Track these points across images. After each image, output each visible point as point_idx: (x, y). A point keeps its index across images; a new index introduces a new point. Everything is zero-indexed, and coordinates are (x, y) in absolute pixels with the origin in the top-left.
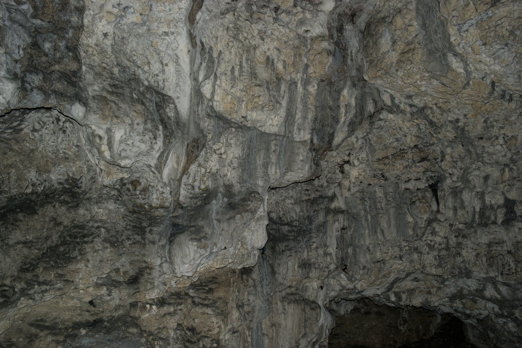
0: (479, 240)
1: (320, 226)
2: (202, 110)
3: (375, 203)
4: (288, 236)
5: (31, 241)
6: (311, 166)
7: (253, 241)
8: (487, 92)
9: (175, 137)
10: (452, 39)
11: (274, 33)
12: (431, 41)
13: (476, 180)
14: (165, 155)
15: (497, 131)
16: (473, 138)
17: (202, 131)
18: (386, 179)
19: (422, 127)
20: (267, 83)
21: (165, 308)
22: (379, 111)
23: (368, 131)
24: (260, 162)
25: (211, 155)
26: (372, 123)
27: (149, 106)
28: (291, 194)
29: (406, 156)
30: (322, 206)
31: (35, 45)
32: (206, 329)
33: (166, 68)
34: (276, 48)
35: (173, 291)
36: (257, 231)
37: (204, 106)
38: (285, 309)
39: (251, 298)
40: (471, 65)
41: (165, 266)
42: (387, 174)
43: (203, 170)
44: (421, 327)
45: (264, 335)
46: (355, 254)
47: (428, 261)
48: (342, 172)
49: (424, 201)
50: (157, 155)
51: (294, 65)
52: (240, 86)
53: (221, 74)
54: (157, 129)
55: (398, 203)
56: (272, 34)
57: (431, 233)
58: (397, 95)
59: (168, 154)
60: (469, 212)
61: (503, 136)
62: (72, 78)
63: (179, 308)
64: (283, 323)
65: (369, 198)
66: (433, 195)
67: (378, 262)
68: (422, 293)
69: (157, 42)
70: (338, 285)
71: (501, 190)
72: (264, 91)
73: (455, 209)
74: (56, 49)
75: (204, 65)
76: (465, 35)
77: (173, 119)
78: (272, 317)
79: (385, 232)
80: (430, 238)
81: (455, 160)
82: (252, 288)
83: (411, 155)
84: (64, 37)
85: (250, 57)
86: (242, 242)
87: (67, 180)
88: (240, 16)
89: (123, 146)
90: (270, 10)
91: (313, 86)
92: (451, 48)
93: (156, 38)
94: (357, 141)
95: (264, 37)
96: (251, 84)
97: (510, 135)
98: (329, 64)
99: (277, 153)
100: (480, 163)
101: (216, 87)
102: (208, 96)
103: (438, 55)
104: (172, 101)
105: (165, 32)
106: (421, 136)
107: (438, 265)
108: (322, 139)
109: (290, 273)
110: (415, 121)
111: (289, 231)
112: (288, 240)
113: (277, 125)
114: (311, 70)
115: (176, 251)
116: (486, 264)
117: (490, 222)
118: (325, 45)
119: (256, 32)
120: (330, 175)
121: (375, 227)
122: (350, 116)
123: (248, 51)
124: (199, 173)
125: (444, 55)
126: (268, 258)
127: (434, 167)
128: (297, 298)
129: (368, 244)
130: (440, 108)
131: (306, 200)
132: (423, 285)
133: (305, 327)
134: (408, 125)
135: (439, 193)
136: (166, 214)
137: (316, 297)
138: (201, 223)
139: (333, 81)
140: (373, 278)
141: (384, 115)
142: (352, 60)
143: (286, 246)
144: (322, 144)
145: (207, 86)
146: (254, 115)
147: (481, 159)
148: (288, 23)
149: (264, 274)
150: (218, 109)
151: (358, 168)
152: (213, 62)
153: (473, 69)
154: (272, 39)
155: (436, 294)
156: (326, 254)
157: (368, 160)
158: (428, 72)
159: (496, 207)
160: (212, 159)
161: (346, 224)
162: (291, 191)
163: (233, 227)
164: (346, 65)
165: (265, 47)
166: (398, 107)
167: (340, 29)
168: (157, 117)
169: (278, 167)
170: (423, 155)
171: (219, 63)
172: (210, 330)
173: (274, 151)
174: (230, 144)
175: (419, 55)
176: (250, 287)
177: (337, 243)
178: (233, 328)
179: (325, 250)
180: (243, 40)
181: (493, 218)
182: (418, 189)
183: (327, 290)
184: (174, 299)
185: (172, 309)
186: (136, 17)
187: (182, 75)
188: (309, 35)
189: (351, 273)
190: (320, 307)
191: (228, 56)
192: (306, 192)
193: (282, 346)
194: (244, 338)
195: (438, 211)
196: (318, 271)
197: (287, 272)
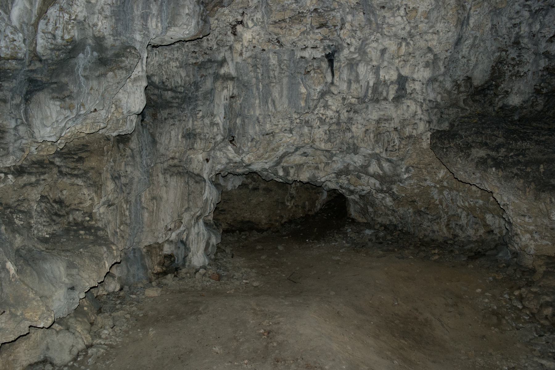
3: (268, 71)
6: (198, 22)
13: (373, 53)
16: (375, 6)
18: (281, 46)
21: (25, 178)
28: (176, 56)
30: (211, 71)
32: (76, 202)
35: (34, 159)
36: (134, 93)
39: (129, 169)
41: (22, 129)
42: (282, 40)
44: (307, 203)
45: (143, 208)
46: (243, 124)
47: (318, 136)
48: (234, 34)
49: (319, 71)
55: (293, 72)
57: (324, 107)
60: (363, 86)
63: (42, 177)
64: (165, 196)
65: (262, 65)
66: (329, 66)
68: (310, 168)
70: (224, 157)
71: (396, 65)
73: (349, 82)
79: (276, 102)
80: (322, 112)
81: (354, 29)
82: (130, 158)
83: (310, 20)
86: (116, 105)
97: (411, 6)
100: (379, 35)
112: (172, 107)
115: (34, 111)
116: (373, 140)
117: (382, 98)
121: (266, 97)
124: (62, 20)
126: (148, 127)
127: (333, 34)
128: (180, 170)
131: (192, 64)
133: (189, 201)
135: (335, 64)
137: (201, 170)
140: (262, 150)
143: (169, 114)
147: (380, 30)
149: (144, 143)
151: (251, 31)
155: (324, 170)
156: (213, 124)
159: (389, 83)
161: (236, 92)
169: (159, 20)
170: (322, 20)
172: (81, 203)
176: (127, 157)
177: (225, 113)
178: (108, 201)
181: (385, 94)
182: (314, 58)
183: (213, 162)
184: (36, 168)
185: (33, 179)
189: (238, 145)
190: (205, 181)
192: (194, 55)
193: (163, 220)
195: (332, 83)
197: (169, 142)
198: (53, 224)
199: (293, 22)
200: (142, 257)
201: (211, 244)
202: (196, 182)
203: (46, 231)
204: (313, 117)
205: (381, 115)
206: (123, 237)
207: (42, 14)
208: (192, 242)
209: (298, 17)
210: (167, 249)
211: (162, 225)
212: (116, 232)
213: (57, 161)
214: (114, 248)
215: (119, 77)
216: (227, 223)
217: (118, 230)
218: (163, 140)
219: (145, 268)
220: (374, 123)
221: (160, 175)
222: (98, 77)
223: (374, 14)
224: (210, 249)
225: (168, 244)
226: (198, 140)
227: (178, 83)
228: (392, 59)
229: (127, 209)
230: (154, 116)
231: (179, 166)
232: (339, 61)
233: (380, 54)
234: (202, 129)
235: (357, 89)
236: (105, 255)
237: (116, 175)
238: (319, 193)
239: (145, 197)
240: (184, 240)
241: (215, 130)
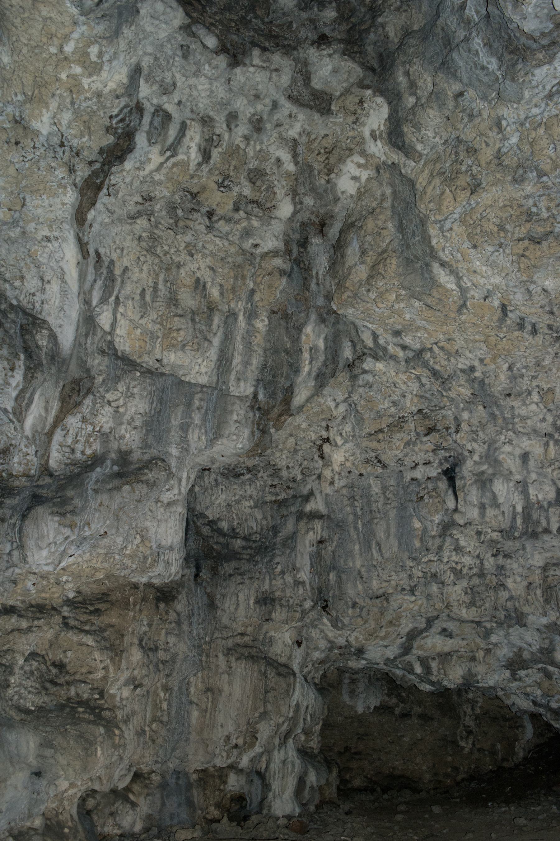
0: (530, 561)
1: (287, 538)
2: (92, 343)
3: (369, 503)
4: (240, 554)
6: (253, 433)
7: (159, 536)
8: (495, 318)
9: (43, 371)
10: (434, 242)
11: (207, 246)
12: (408, 247)
13: (509, 461)
14: (28, 395)
15: (529, 383)
16: (496, 394)
17: (88, 370)
18: (384, 466)
19: (424, 380)
20: (193, 312)
21: (13, 620)
22: (360, 357)
23: (350, 389)
25: (102, 407)
26: (354, 378)
27: (10, 328)
28: (249, 492)
29: (406, 427)
30: (293, 509)
32: (84, 670)
33: (47, 286)
34: (209, 267)
35: (33, 602)
36: (166, 521)
37: (96, 339)
38: (231, 668)
39: (172, 640)
40: (465, 278)
41: (16, 553)
42: (383, 458)
43: (90, 428)
44: (499, 746)
45: (191, 702)
46: (339, 581)
47: (454, 597)
48: (322, 457)
49: (434, 494)
50: (14, 394)
51: (233, 290)
52: (154, 315)
53: (127, 298)
54: (17, 356)
55: (402, 502)
56: (204, 247)
57: (455, 550)
58: (380, 331)
59: (33, 394)
60: (506, 512)
61: (537, 390)
63: (36, 623)
64: (226, 688)
65: (361, 496)
66: (449, 486)
67: (377, 598)
68: (462, 660)
69: (36, 251)
70: (322, 638)
71: (550, 476)
72: (187, 323)
73: (482, 507)
75: (99, 283)
76: (449, 235)
77: (44, 350)
78: (209, 678)
79: (382, 546)
80: (454, 558)
81: (474, 429)
82: (173, 625)
83: (413, 425)
85: (171, 278)
86: (142, 537)
88: (160, 223)
90: (202, 216)
91: (262, 321)
92: (433, 254)
93: (35, 245)
94: (337, 406)
95: (194, 252)
96: (169, 313)
97: (546, 387)
98: (281, 288)
99: (203, 411)
100: (510, 433)
101: (119, 316)
102: (107, 328)
103: (418, 265)
104: (46, 326)
105: (47, 237)
106: (427, 395)
107: (470, 602)
108: (272, 395)
109: (241, 612)
110: (413, 371)
111: (243, 548)
112: (240, 559)
113: (206, 373)
114: (257, 297)
115: (30, 529)
116: (541, 599)
117: (540, 530)
118: (278, 262)
119: (183, 245)
120: (306, 463)
121: (368, 540)
122: (318, 364)
123: (168, 269)
124: (84, 432)
125: (427, 265)
126: (204, 584)
127: (446, 441)
128: (253, 652)
129: (358, 566)
130: (442, 348)
131: (271, 502)
132: (464, 647)
133: (265, 702)
134: (404, 377)
135: (458, 483)
136: (28, 484)
137: (290, 658)
138: (70, 493)
139: (290, 312)
140: (372, 624)
141: (368, 364)
142: (318, 284)
143: (235, 569)
144: (272, 402)
145: (105, 314)
146: (172, 357)
147: (510, 426)
148: (228, 234)
150: (122, 348)
151: (343, 450)
152: (113, 281)
153: (469, 284)
154: (204, 254)
155: (484, 661)
156: (298, 583)
157: (354, 436)
158: (405, 289)
159: (545, 504)
160: (102, 412)
161: (325, 534)
162: (248, 487)
163: (117, 501)
164: (308, 290)
165: (193, 266)
166: (385, 349)
167: (304, 243)
168: (18, 342)
169: (203, 431)
170: (427, 423)
171: (123, 282)
172: (90, 673)
173: (198, 409)
174: (133, 395)
175: (394, 266)
176: (171, 623)
177: (311, 564)
178: (134, 679)
179: (295, 576)
180: (161, 255)
181: (544, 523)
182: (429, 478)
183: (308, 647)
184: (32, 612)
185: (24, 624)
186: (4, 212)
187: (69, 296)
188: (259, 251)
189: (334, 614)
190: (294, 674)
191: (137, 274)
192: (273, 490)
193: (222, 726)
194: (156, 701)
195: (456, 510)
196: (285, 610)
197: (236, 609)
198: (44, 692)
199: (392, 431)
200: (189, 786)
201: (308, 784)
202: (279, 674)
203: (33, 702)
204: (442, 566)
205: (546, 558)
206: (153, 741)
207: (58, 421)
208: (275, 774)
209: (399, 423)
210: (234, 783)
211: (219, 734)
212: (144, 732)
213: (66, 611)
214: (117, 732)
215: (137, 492)
216: (367, 777)
217: (147, 729)
218: (227, 605)
219: (190, 804)
220: (538, 571)
221: (220, 655)
222: (111, 490)
223: (498, 406)
224: (306, 793)
225: (236, 773)
226: (278, 607)
227: (252, 528)
228: (542, 468)
229: (165, 700)
230: (214, 571)
231: (251, 647)
232: (462, 478)
233: (520, 462)
234: (283, 591)
235: (495, 516)
236: (100, 739)
237: (152, 646)
238: (517, 728)
239: (196, 684)
240: (263, 771)
241: (301, 591)
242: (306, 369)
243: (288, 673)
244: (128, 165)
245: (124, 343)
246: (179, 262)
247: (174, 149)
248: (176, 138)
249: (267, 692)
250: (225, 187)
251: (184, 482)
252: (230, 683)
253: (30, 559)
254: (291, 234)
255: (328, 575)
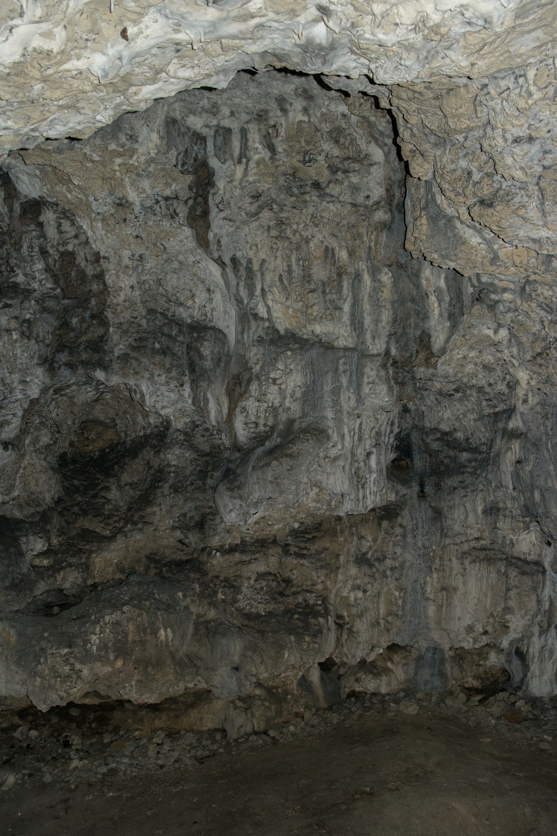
2: (248, 337)
5: (136, 483)
11: (324, 215)
24: (328, 388)
31: (65, 325)
32: (309, 583)
36: (334, 473)
43: (266, 405)
45: (427, 599)
62: (98, 346)
64: (461, 587)
74: (83, 320)
78: (444, 578)
84: (88, 308)
87: (162, 423)
89: (154, 398)
99: (348, 374)
111: (470, 461)
112: (463, 473)
123: (298, 248)
126: (429, 499)
131: (489, 415)
137: (540, 555)
139: (403, 262)
146: (318, 329)
172: (313, 585)
173: (344, 372)
176: (397, 536)
196: (508, 520)
198: (273, 602)
206: (388, 630)
212: (378, 623)
221: (454, 559)
230: (438, 487)
239: (432, 583)
242: (437, 312)
243: (538, 571)
244: (221, 184)
245: (283, 324)
246: (307, 237)
247: (244, 157)
248: (241, 147)
249: (508, 590)
250: (310, 161)
251: (347, 438)
252: (465, 583)
253: (225, 520)
254: (392, 175)
255: (533, 493)
